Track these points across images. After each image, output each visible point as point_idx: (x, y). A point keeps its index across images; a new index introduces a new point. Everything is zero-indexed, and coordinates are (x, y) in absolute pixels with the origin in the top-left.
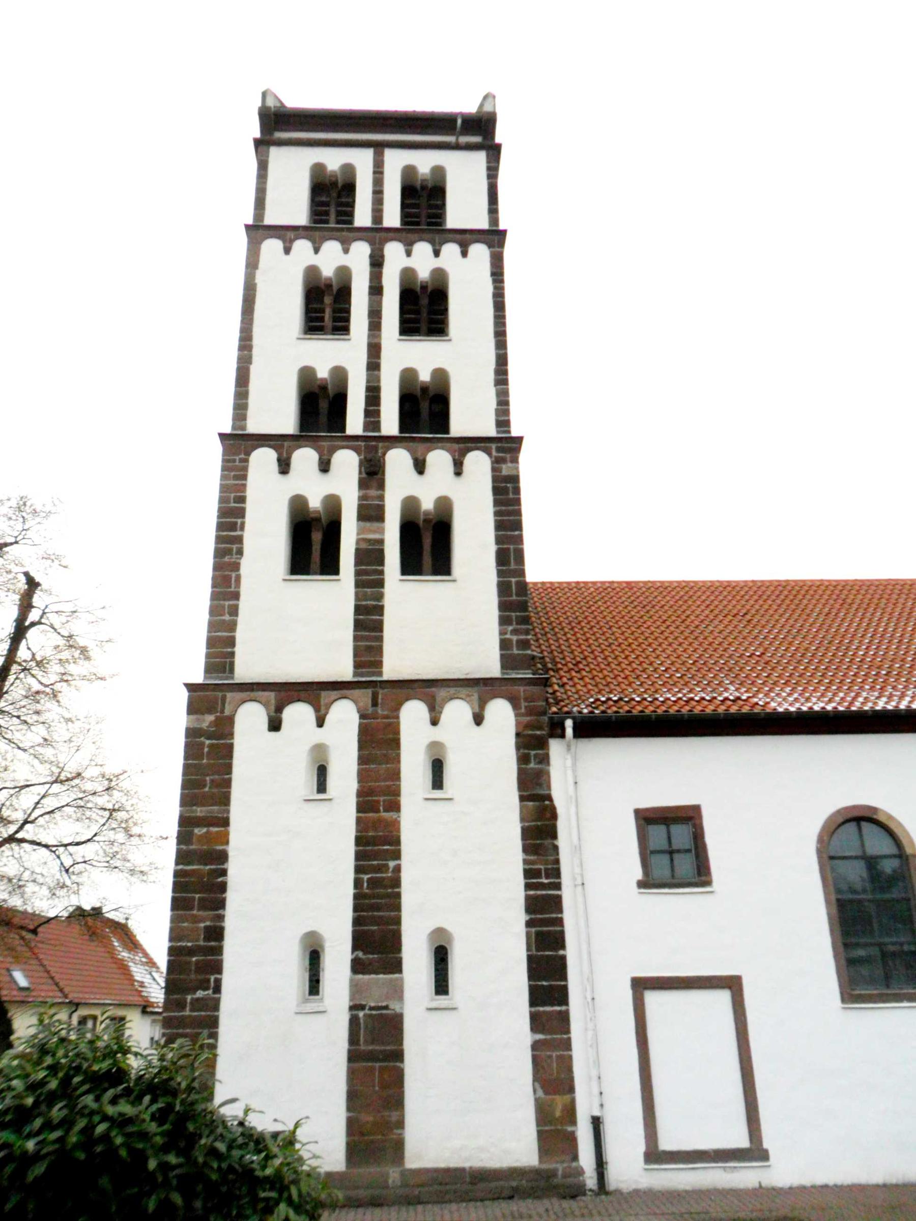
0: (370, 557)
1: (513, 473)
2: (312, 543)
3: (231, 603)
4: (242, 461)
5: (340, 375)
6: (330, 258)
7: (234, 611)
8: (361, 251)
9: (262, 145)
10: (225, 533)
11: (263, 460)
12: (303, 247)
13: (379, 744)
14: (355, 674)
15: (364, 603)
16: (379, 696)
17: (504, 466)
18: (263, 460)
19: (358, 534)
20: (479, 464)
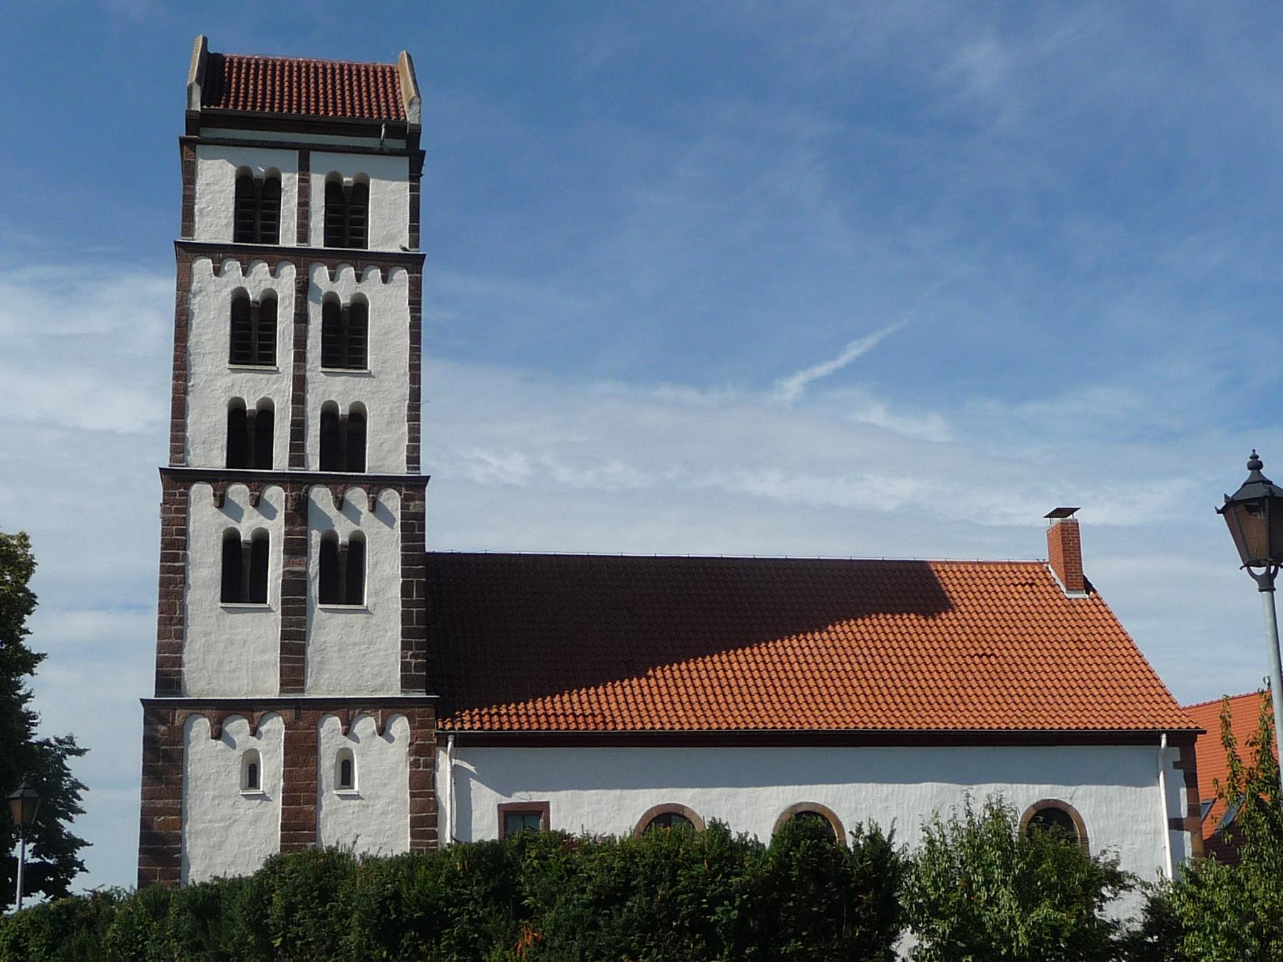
0: (294, 586)
2: (242, 574)
5: (266, 412)
6: (258, 281)
8: (289, 272)
9: (188, 144)
11: (201, 494)
13: (301, 752)
14: (282, 691)
16: (303, 714)
18: (201, 494)
20: (392, 500)
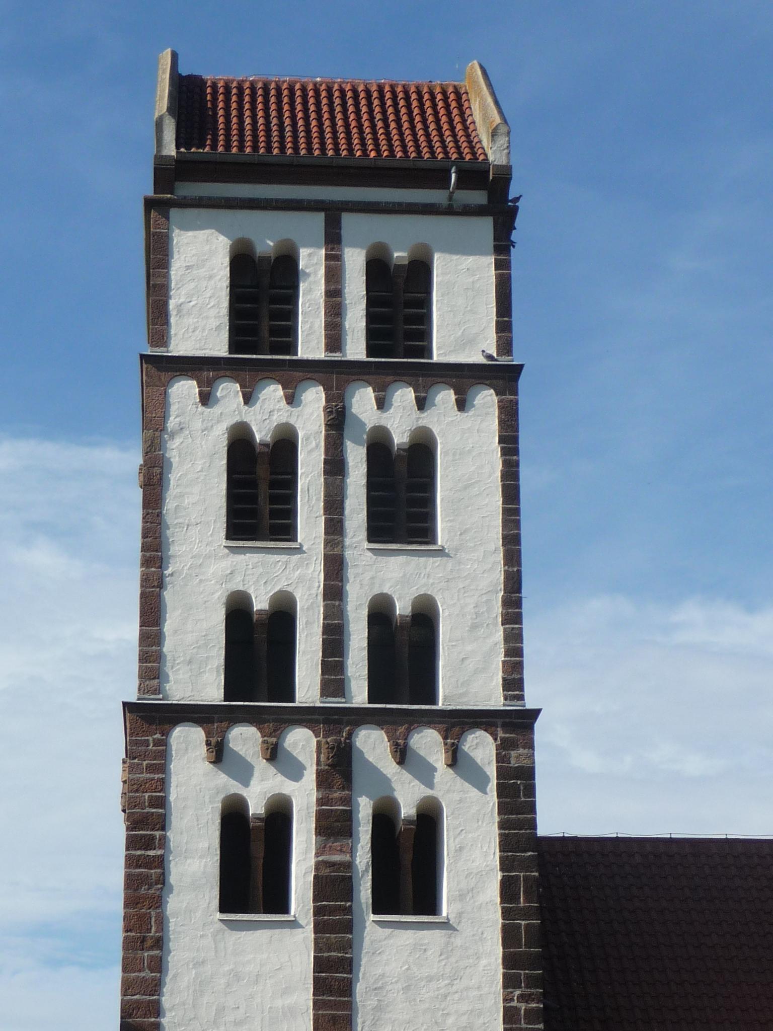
0: (332, 886)
1: (525, 762)
2: (251, 870)
3: (152, 953)
4: (157, 743)
6: (268, 411)
7: (158, 965)
8: (314, 398)
10: (139, 853)
12: (229, 391)
15: (326, 955)
17: (513, 753)
19: (317, 855)
20: (482, 747)
